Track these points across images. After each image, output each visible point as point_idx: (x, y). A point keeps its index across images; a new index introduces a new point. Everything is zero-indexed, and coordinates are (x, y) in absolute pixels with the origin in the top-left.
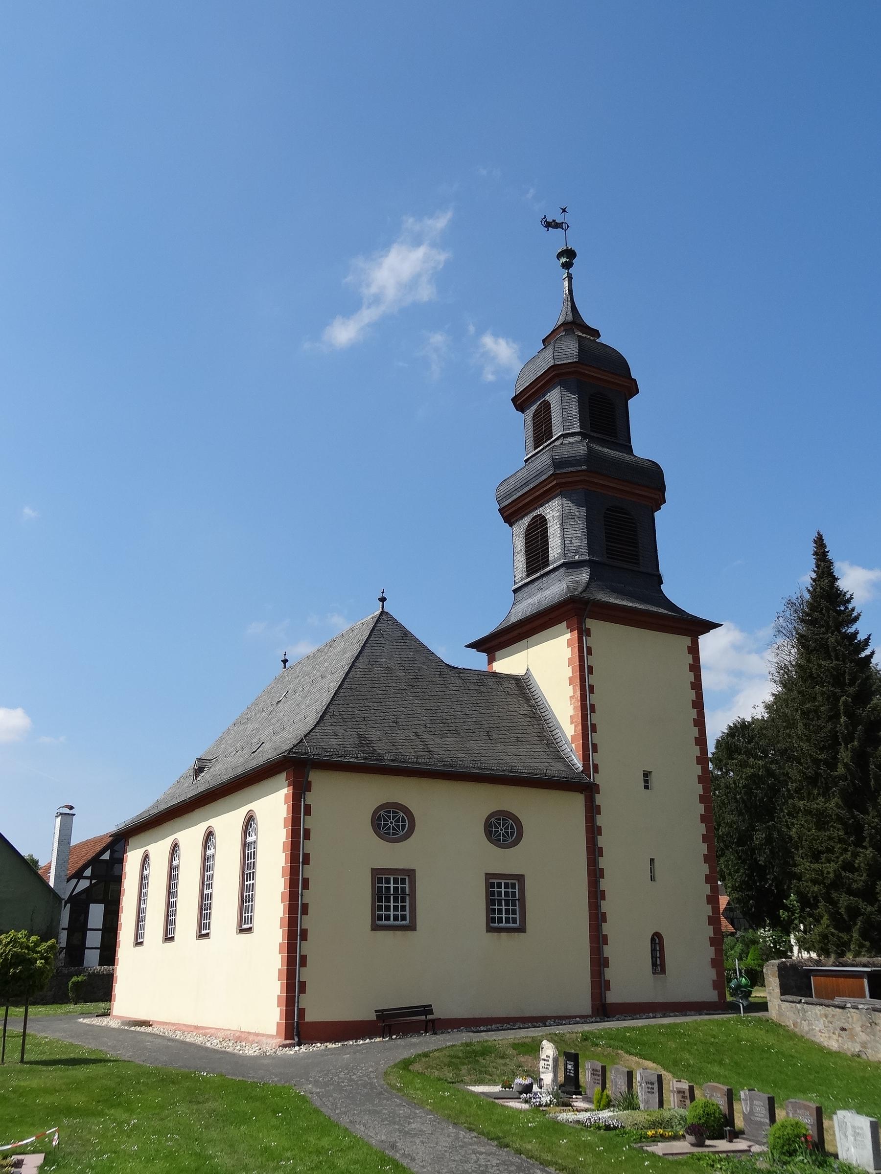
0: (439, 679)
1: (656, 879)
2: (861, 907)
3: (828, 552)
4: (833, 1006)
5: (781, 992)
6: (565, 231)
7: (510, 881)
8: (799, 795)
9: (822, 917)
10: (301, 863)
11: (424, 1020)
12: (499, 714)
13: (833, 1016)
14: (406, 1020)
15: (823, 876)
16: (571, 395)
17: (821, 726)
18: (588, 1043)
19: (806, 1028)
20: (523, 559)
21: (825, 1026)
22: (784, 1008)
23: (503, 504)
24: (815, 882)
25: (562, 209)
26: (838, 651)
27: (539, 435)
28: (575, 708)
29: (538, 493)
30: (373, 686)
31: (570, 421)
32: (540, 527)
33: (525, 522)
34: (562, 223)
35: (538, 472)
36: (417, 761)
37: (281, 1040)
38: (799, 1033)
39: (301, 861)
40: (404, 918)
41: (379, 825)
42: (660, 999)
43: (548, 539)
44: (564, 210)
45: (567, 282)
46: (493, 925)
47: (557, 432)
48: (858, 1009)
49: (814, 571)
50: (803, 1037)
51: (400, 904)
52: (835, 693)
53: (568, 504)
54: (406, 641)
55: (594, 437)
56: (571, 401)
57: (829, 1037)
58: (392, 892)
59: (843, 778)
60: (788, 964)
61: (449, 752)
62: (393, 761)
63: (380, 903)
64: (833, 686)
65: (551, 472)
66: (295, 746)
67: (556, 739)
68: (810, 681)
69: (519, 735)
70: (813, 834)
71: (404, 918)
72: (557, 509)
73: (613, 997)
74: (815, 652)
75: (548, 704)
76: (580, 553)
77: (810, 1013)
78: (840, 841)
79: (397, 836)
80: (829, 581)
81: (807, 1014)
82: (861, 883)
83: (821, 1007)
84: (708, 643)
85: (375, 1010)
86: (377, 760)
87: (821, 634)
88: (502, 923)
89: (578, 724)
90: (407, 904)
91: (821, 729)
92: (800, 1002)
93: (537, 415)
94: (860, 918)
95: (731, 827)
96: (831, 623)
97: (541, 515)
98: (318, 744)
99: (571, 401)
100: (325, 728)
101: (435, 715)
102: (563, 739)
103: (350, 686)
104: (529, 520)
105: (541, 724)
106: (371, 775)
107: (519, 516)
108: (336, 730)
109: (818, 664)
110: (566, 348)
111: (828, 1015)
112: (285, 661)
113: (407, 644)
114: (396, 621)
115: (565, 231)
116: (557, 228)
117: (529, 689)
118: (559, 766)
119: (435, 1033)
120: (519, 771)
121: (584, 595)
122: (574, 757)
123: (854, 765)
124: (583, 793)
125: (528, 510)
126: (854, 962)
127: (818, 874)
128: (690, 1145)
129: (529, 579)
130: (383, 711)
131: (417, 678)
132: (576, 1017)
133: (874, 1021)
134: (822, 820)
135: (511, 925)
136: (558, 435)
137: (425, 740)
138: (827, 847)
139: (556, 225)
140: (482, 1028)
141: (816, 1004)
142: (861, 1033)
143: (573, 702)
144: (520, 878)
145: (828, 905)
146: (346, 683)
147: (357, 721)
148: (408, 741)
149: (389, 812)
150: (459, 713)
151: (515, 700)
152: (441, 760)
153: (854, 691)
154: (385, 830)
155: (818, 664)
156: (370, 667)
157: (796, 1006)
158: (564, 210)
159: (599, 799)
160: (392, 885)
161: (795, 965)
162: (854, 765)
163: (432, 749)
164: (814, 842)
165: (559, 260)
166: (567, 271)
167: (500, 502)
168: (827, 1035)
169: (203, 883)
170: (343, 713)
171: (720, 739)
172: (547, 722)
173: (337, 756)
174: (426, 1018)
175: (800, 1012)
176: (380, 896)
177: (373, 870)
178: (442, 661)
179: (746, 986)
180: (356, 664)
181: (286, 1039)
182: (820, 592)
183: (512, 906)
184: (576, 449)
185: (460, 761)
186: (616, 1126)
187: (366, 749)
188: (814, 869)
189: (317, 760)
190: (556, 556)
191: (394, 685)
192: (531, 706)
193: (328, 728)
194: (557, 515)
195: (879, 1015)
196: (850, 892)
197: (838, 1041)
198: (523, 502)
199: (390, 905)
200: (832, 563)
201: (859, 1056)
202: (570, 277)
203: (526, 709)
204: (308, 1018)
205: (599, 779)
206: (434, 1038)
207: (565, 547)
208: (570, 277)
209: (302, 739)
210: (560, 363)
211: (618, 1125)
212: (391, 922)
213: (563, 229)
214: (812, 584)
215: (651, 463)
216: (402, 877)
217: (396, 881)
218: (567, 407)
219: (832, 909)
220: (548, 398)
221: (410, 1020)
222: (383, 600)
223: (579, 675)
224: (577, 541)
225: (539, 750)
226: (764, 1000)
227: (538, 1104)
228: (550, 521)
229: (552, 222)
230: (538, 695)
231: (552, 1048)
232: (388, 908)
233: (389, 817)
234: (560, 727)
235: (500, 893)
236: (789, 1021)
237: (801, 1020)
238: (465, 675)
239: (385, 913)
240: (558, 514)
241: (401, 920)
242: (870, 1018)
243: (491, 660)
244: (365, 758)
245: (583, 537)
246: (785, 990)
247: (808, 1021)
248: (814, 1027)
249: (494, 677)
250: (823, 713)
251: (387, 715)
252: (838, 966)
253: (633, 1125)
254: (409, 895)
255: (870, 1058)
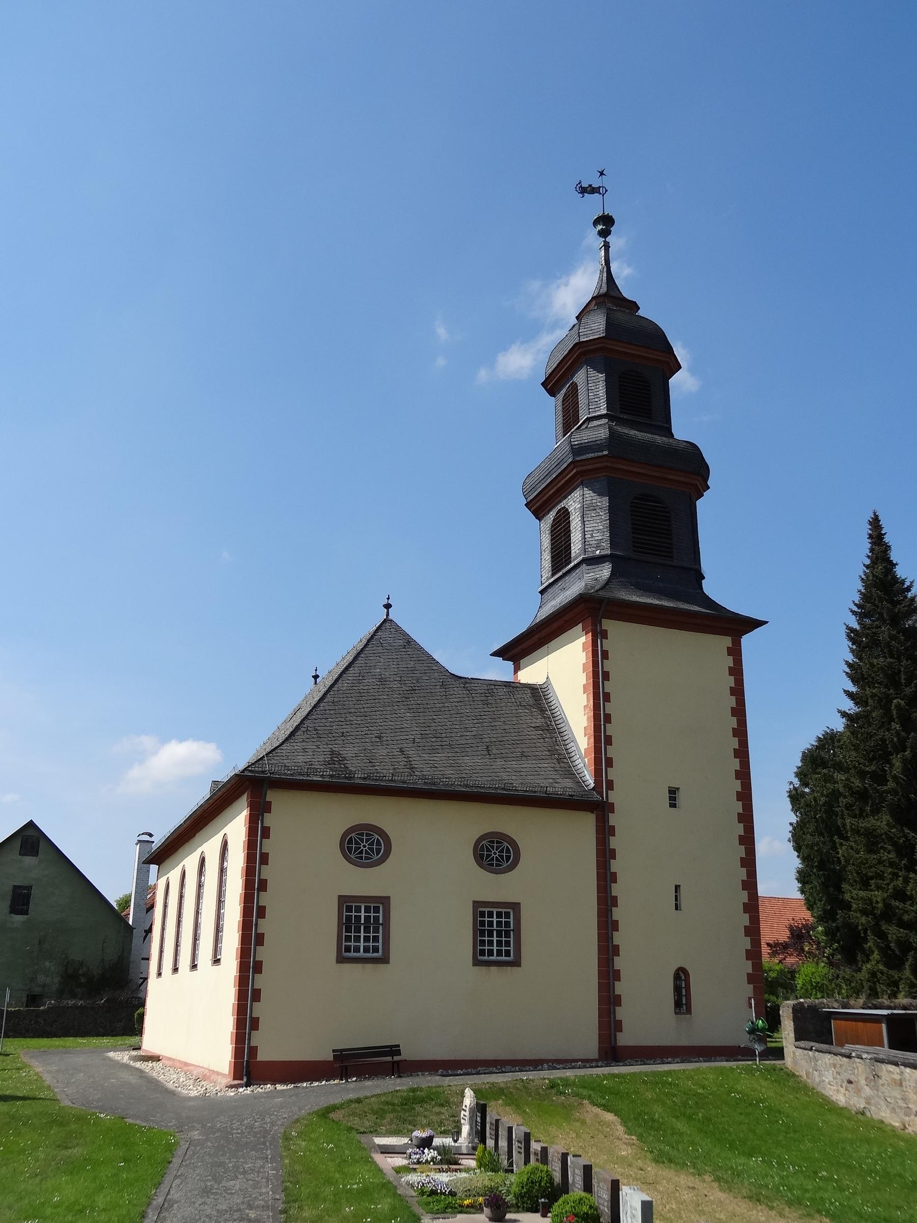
0: (441, 690)
1: (683, 907)
2: (912, 941)
3: (885, 534)
4: (840, 1055)
5: (795, 1037)
6: (603, 196)
7: (503, 910)
8: (850, 812)
9: (873, 952)
10: (256, 890)
11: (391, 1061)
12: (506, 727)
13: (841, 1066)
14: (367, 1061)
15: (872, 905)
16: (598, 374)
17: (872, 734)
18: (554, 1091)
19: (817, 1080)
20: (548, 557)
21: (833, 1078)
22: (798, 1056)
23: (530, 499)
24: (864, 912)
25: (599, 172)
26: (892, 647)
27: (567, 421)
28: (588, 718)
29: (560, 484)
30: (360, 698)
31: (597, 403)
32: (564, 522)
33: (551, 517)
34: (600, 187)
35: (559, 461)
36: (392, 778)
37: (229, 1080)
38: (811, 1084)
39: (256, 887)
40: (376, 950)
41: (482, 856)
42: (684, 1042)
43: (570, 534)
44: (602, 173)
45: (603, 251)
46: (481, 958)
47: (583, 416)
48: (862, 1058)
49: (868, 557)
50: (813, 1089)
51: (371, 935)
52: (889, 695)
53: (588, 493)
54: (408, 650)
55: (623, 419)
56: (597, 381)
57: (838, 1091)
58: (362, 922)
59: (894, 792)
60: (806, 1005)
61: (435, 769)
62: (364, 778)
63: (348, 933)
64: (886, 686)
65: (570, 460)
66: (253, 764)
67: (569, 753)
68: (861, 683)
69: (525, 750)
70: (862, 857)
71: (376, 950)
72: (578, 500)
73: (624, 1039)
74: (867, 649)
75: (564, 714)
76: (602, 548)
77: (820, 1061)
78: (891, 864)
79: (370, 861)
80: (885, 567)
81: (818, 1063)
82: (913, 914)
83: (830, 1055)
84: (747, 641)
85: (333, 1050)
86: (346, 778)
87: (874, 628)
88: (493, 956)
89: (591, 736)
90: (380, 935)
91: (871, 737)
92: (811, 1049)
93: (567, 398)
94: (912, 953)
95: (812, 848)
96: (885, 615)
97: (564, 507)
98: (281, 761)
99: (597, 381)
100: (295, 744)
101: (427, 729)
102: (577, 754)
103: (332, 699)
104: (554, 515)
105: (554, 737)
106: (365, 796)
107: (546, 511)
108: (306, 747)
109: (870, 663)
110: (593, 323)
111: (836, 1064)
112: (316, 677)
113: (408, 653)
114: (401, 629)
115: (603, 196)
116: (594, 194)
117: (546, 699)
118: (568, 783)
119: (400, 1077)
120: (514, 788)
121: (600, 593)
122: (586, 772)
123: (905, 778)
124: (594, 813)
125: (554, 503)
126: (892, 1004)
127: (867, 904)
128: (488, 1219)
129: (553, 579)
130: (368, 725)
131: (413, 690)
132: (577, 1061)
133: (877, 1073)
134: (873, 841)
135: (504, 958)
136: (584, 419)
137: (410, 756)
138: (876, 873)
139: (593, 190)
140: (459, 1072)
141: (825, 1052)
142: (865, 1087)
143: (586, 711)
144: (516, 906)
145: (876, 938)
146: (328, 696)
147: (334, 737)
148: (390, 757)
149: (493, 842)
150: (457, 727)
151: (527, 711)
152: (424, 777)
153: (910, 692)
154: (356, 855)
155: (870, 663)
156: (361, 678)
157: (808, 1053)
158: (602, 173)
159: (613, 819)
160: (363, 914)
161: (815, 1006)
162: (905, 778)
163: (416, 766)
164: (863, 866)
165: (595, 227)
166: (604, 239)
167: (527, 496)
168: (835, 1088)
169: (197, 911)
170: (319, 728)
171: (806, 751)
172: (563, 734)
173: (300, 774)
174: (393, 1059)
175: (812, 1060)
176: (481, 929)
177: (340, 897)
178: (447, 670)
179: (762, 1030)
180: (345, 675)
181: (234, 1079)
182: (873, 580)
183: (485, 940)
184: (596, 433)
185: (446, 778)
186: (444, 1191)
187: (336, 766)
188: (862, 898)
189: (274, 779)
190: (577, 552)
191: (385, 697)
192: (545, 718)
193: (298, 744)
194: (578, 506)
195: (881, 1067)
196: (902, 924)
197: (845, 1095)
198: (548, 495)
199: (360, 936)
200: (890, 546)
201: (863, 1114)
202: (607, 246)
203: (539, 721)
204: (261, 1057)
205: (614, 797)
206: (398, 1081)
207: (585, 542)
208: (607, 246)
209: (264, 757)
210: (585, 340)
211: (446, 1191)
212: (361, 953)
213: (600, 194)
214: (865, 572)
215: (688, 445)
216: (347, 904)
217: (367, 910)
218: (593, 388)
219: (882, 943)
220: (575, 379)
221: (370, 1061)
222: (388, 606)
223: (592, 682)
224: (598, 534)
225: (546, 765)
226: (802, 1044)
227: (415, 1161)
228: (572, 514)
229: (588, 187)
230: (556, 705)
231: (471, 1097)
232: (357, 939)
233: (362, 840)
234: (574, 741)
235: (491, 924)
236: (802, 1071)
237: (813, 1071)
238: (472, 685)
239: (354, 944)
240: (579, 505)
241: (373, 952)
242: (874, 1070)
243: (517, 669)
244: (331, 776)
245: (605, 530)
246: (800, 1035)
247: (819, 1071)
248: (824, 1079)
249: (506, 686)
250: (875, 719)
251: (371, 730)
252: (870, 1008)
253: (466, 1191)
254: (382, 924)
255: (873, 1116)
